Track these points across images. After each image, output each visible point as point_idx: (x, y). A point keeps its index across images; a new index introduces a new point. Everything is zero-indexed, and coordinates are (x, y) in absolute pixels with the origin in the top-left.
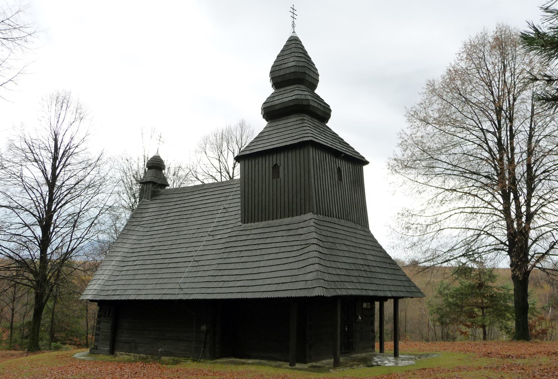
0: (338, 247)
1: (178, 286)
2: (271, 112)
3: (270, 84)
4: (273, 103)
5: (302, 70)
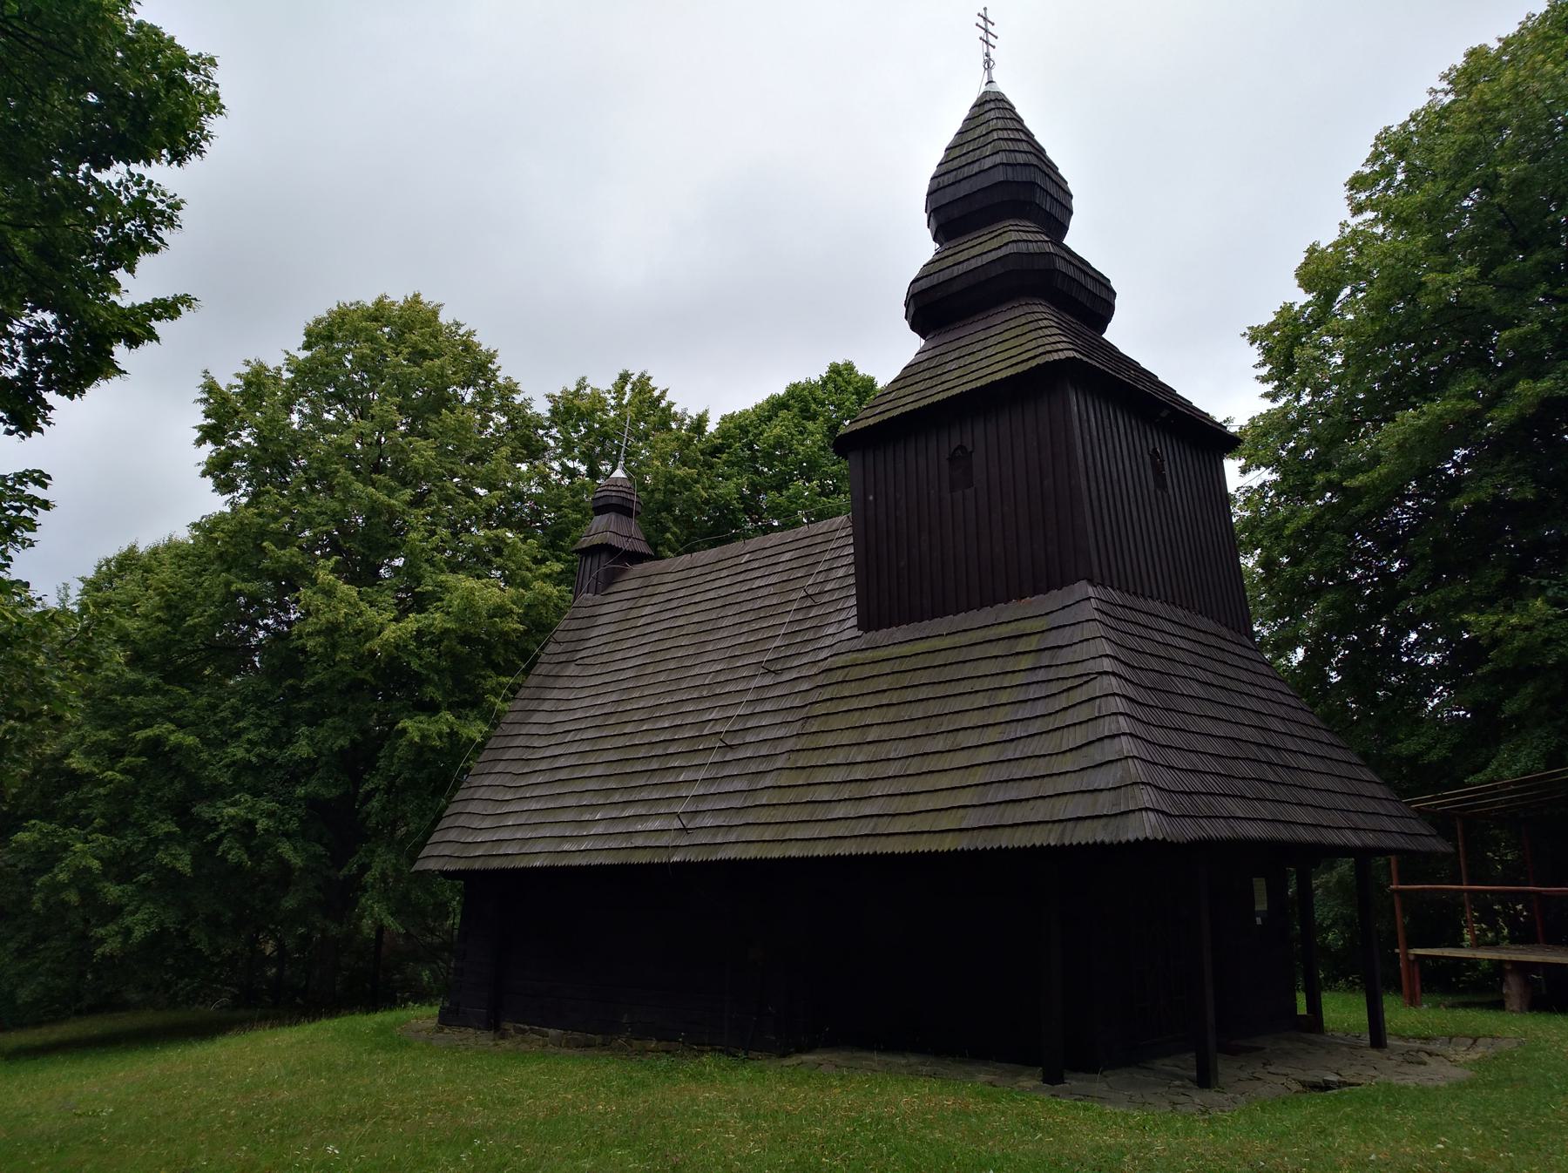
0: (1181, 686)
1: (677, 824)
2: (930, 307)
3: (928, 234)
5: (1023, 176)
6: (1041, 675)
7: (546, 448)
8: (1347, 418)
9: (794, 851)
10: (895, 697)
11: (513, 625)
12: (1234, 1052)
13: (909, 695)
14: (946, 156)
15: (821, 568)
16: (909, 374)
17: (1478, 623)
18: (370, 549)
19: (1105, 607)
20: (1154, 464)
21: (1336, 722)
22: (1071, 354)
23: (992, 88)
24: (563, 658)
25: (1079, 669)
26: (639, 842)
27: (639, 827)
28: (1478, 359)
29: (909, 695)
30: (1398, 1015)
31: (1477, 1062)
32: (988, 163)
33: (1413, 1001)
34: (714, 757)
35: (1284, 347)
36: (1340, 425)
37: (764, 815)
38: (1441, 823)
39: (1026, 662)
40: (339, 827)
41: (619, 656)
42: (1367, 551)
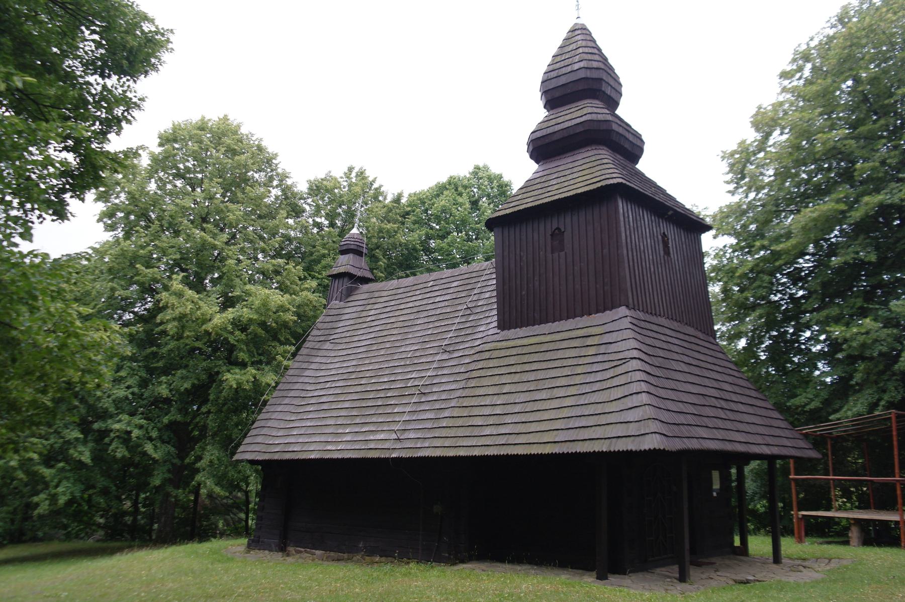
1: (394, 436)
2: (544, 148)
3: (541, 104)
4: (549, 131)
5: (595, 75)
6: (600, 358)
7: (304, 211)
8: (774, 209)
9: (462, 453)
10: (519, 368)
11: (290, 317)
12: (699, 565)
13: (527, 367)
14: (553, 60)
15: (476, 291)
16: (529, 185)
17: (837, 331)
18: (202, 268)
19: (635, 321)
20: (663, 241)
21: (759, 383)
22: (620, 180)
23: (579, 21)
24: (322, 338)
25: (621, 356)
26: (372, 446)
27: (372, 438)
28: (847, 176)
29: (527, 367)
30: (788, 545)
31: (828, 571)
32: (576, 67)
33: (800, 540)
34: (415, 399)
35: (741, 165)
36: (774, 209)
37: (444, 432)
38: (818, 442)
39: (592, 351)
40: (182, 437)
41: (356, 339)
42: (783, 284)
